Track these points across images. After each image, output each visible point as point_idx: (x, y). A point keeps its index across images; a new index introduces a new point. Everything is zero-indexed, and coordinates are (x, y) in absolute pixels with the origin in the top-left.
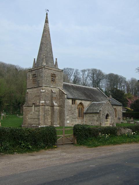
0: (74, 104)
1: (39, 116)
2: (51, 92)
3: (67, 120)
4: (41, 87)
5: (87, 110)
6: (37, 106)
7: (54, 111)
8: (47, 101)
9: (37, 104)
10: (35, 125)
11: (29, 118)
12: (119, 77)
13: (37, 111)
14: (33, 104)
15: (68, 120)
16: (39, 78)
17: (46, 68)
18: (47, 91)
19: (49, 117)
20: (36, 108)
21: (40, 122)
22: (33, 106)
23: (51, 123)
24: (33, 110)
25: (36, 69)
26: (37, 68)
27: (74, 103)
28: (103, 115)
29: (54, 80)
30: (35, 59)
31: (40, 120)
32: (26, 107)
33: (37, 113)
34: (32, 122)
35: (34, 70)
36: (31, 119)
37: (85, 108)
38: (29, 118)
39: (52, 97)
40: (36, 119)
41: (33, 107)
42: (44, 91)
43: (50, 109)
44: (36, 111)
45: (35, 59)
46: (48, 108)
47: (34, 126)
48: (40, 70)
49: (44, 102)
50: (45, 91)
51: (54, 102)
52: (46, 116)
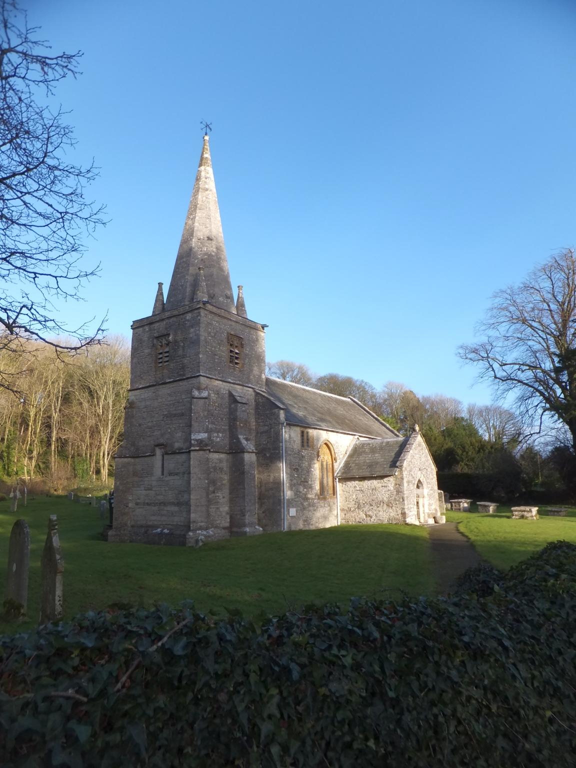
0: (308, 446)
1: (188, 490)
2: (227, 400)
3: (288, 506)
4: (194, 381)
5: (347, 465)
6: (174, 453)
7: (243, 473)
8: (216, 434)
9: (177, 445)
10: (166, 531)
11: (137, 504)
12: (358, 383)
13: (177, 474)
14: (157, 445)
15: (293, 507)
16: (183, 347)
17: (211, 312)
18: (213, 396)
19: (223, 496)
20: (172, 462)
21: (192, 515)
22: (159, 452)
23: (231, 517)
24: (158, 471)
25: (167, 314)
26: (176, 313)
27: (305, 444)
28: (408, 482)
29: (237, 358)
30: (160, 284)
31: (192, 508)
32: (126, 460)
33: (176, 481)
34: (153, 518)
35: (163, 320)
36: (148, 504)
37: (338, 461)
38: (137, 504)
39: (233, 419)
40: (173, 504)
41: (157, 460)
42: (205, 394)
43: (225, 465)
44: (170, 474)
45: (160, 284)
46: (221, 461)
47: (161, 533)
48: (189, 316)
49: (206, 435)
50: (209, 395)
51: (241, 437)
52: (214, 492)
